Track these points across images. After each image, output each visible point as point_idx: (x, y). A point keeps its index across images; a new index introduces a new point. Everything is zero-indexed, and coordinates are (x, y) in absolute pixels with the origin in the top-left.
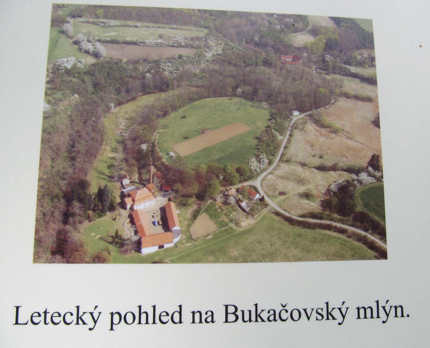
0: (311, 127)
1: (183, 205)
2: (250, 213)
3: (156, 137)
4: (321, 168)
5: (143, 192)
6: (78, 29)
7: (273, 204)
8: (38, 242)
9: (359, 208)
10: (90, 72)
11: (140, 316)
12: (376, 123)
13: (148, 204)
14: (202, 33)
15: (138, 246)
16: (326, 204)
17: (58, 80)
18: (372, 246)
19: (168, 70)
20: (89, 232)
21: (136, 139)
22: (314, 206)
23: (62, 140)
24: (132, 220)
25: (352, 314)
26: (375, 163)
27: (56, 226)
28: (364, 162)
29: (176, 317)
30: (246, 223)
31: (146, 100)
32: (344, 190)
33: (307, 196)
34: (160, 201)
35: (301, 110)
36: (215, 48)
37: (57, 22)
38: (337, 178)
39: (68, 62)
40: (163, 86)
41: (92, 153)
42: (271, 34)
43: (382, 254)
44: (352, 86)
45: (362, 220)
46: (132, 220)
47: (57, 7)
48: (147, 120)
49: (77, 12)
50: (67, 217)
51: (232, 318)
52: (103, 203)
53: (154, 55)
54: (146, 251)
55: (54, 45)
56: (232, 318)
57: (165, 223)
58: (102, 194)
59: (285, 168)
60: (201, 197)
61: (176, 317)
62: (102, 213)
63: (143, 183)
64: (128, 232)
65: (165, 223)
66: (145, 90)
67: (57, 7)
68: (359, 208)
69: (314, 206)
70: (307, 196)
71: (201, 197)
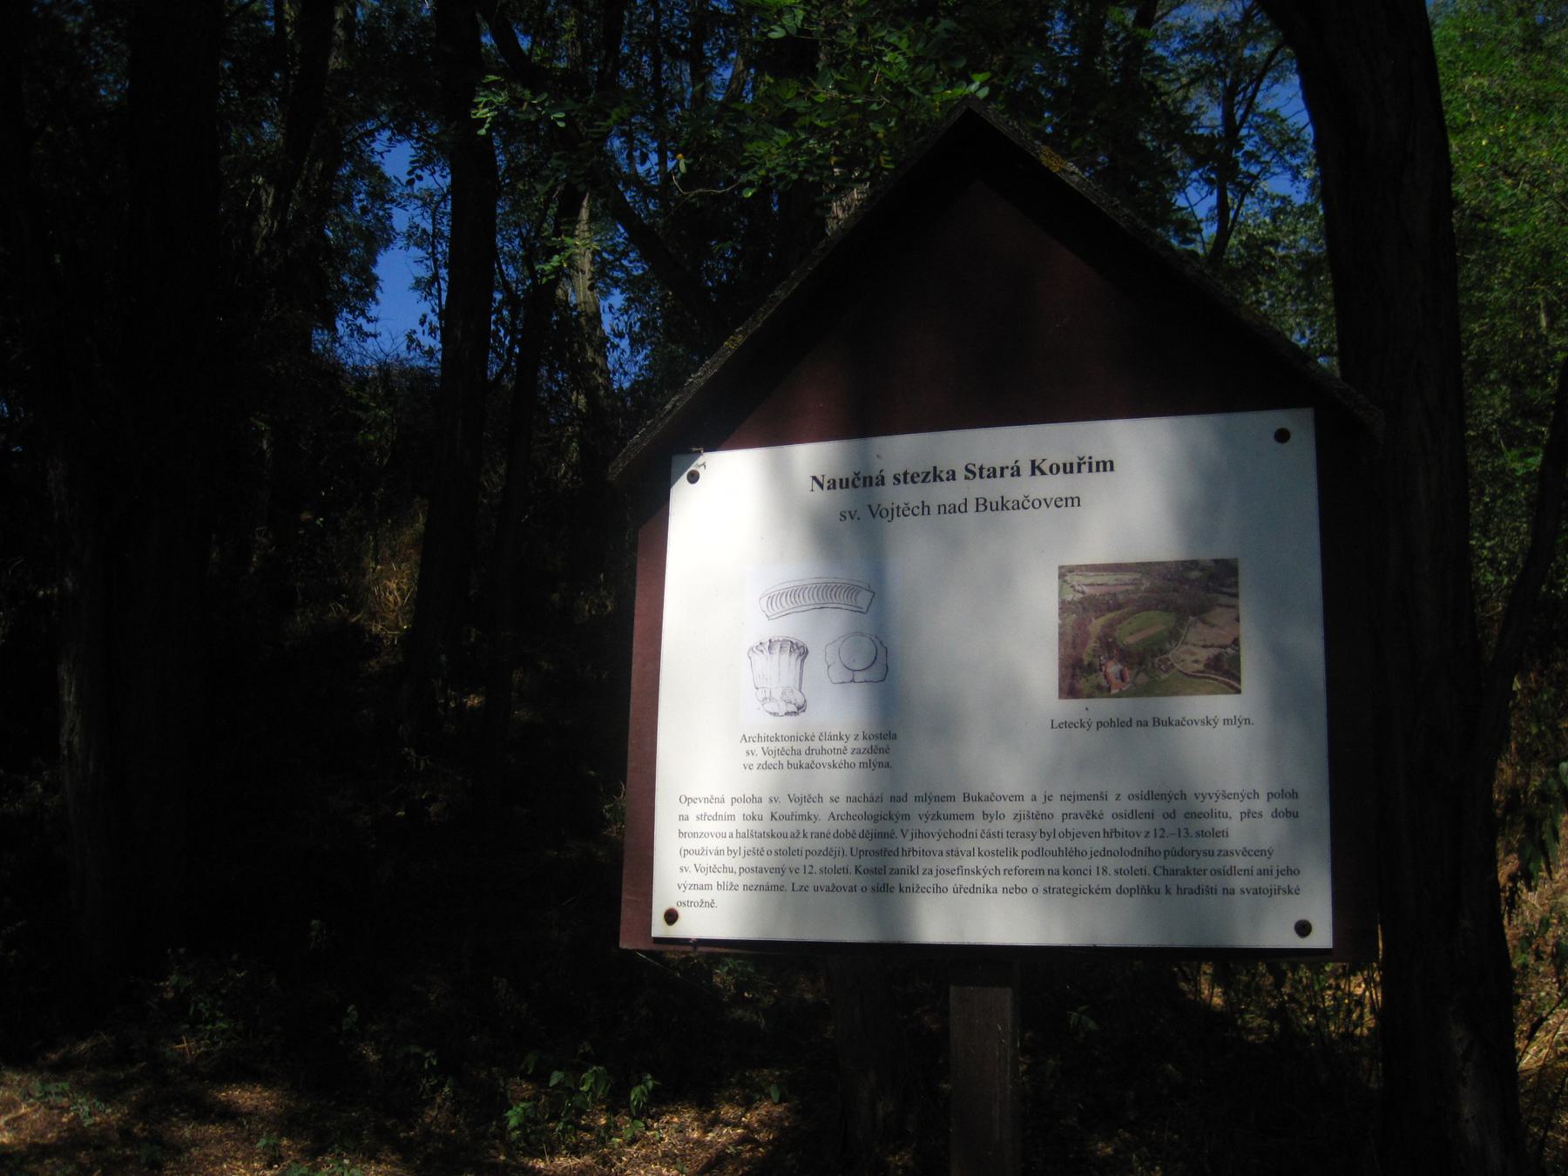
0: (1199, 625)
1: (1131, 668)
2: (1166, 672)
3: (1116, 634)
4: (1205, 647)
5: (1110, 663)
6: (1074, 579)
7: (1178, 666)
8: (1061, 689)
9: (1226, 667)
10: (1081, 602)
11: (1111, 723)
12: (1238, 620)
13: (1113, 668)
14: (1138, 576)
15: (1109, 690)
16: (1206, 666)
17: (1065, 607)
18: (1232, 687)
19: (1121, 598)
20: (1082, 684)
21: (1106, 636)
22: (1200, 667)
23: (1069, 638)
24: (1106, 676)
25: (1221, 723)
26: (1236, 642)
27: (1068, 681)
28: (1229, 641)
29: (1129, 724)
30: (1164, 676)
31: (1110, 615)
32: (1218, 658)
33: (1196, 661)
34: (1120, 667)
35: (1194, 615)
36: (1146, 584)
37: (1062, 576)
38: (1213, 652)
39: (1069, 597)
40: (1119, 607)
41: (1084, 644)
42: (1497, 55)
43: (1238, 691)
44: (1223, 599)
45: (1227, 674)
46: (1106, 676)
47: (1061, 568)
48: (1111, 626)
49: (1072, 569)
50: (1073, 676)
51: (981, 508)
52: (1091, 669)
53: (1113, 590)
54: (1114, 691)
55: (1061, 588)
56: (981, 508)
57: (1122, 678)
58: (1090, 664)
59: (1186, 647)
60: (1140, 664)
61: (1129, 724)
62: (1090, 673)
63: (1111, 658)
64: (1104, 683)
65: (1122, 678)
66: (1109, 610)
67: (1061, 568)
68: (1226, 667)
69: (1200, 667)
70: (1196, 661)
71: (1140, 664)
